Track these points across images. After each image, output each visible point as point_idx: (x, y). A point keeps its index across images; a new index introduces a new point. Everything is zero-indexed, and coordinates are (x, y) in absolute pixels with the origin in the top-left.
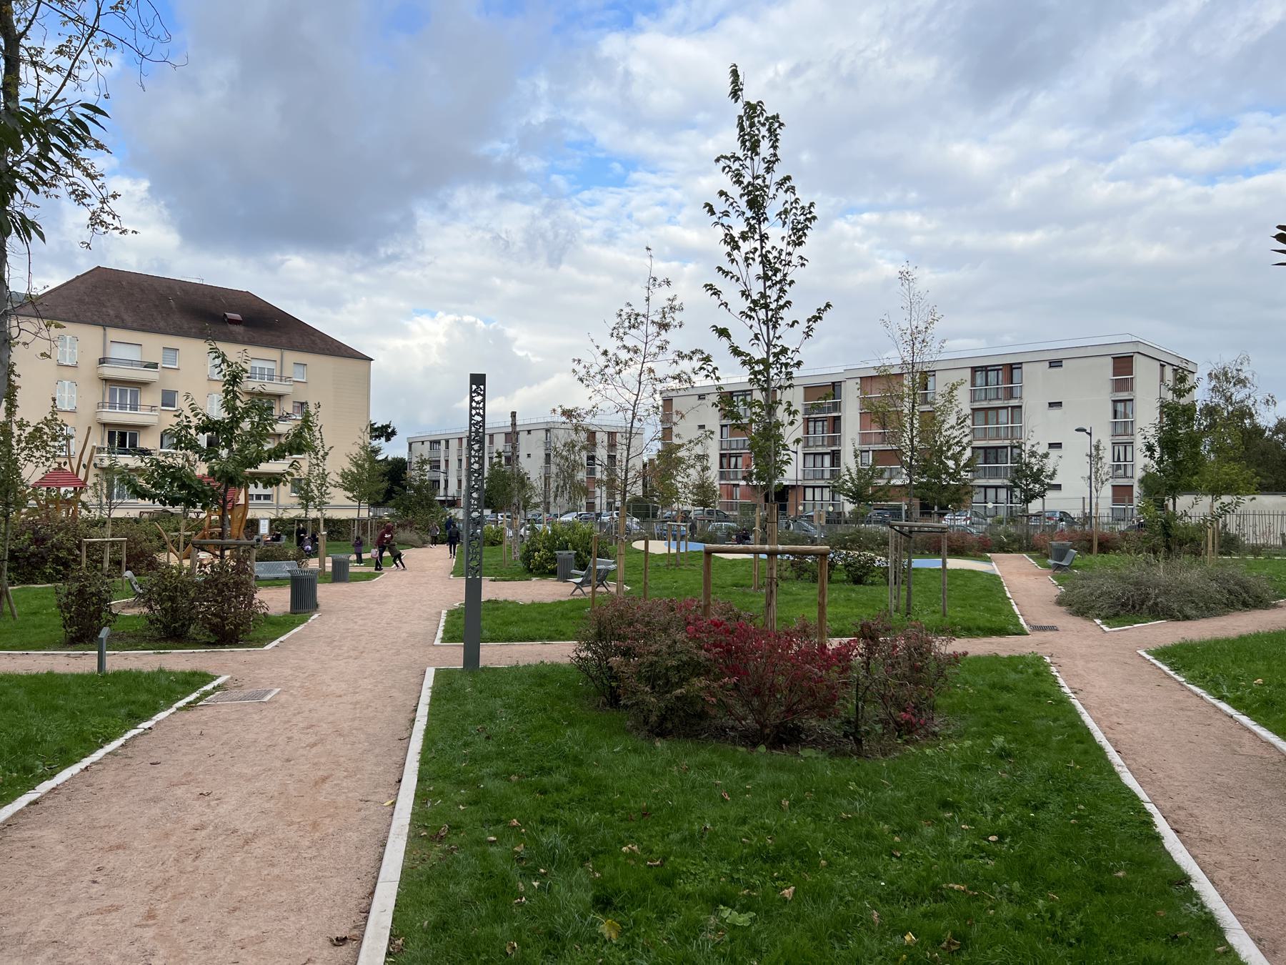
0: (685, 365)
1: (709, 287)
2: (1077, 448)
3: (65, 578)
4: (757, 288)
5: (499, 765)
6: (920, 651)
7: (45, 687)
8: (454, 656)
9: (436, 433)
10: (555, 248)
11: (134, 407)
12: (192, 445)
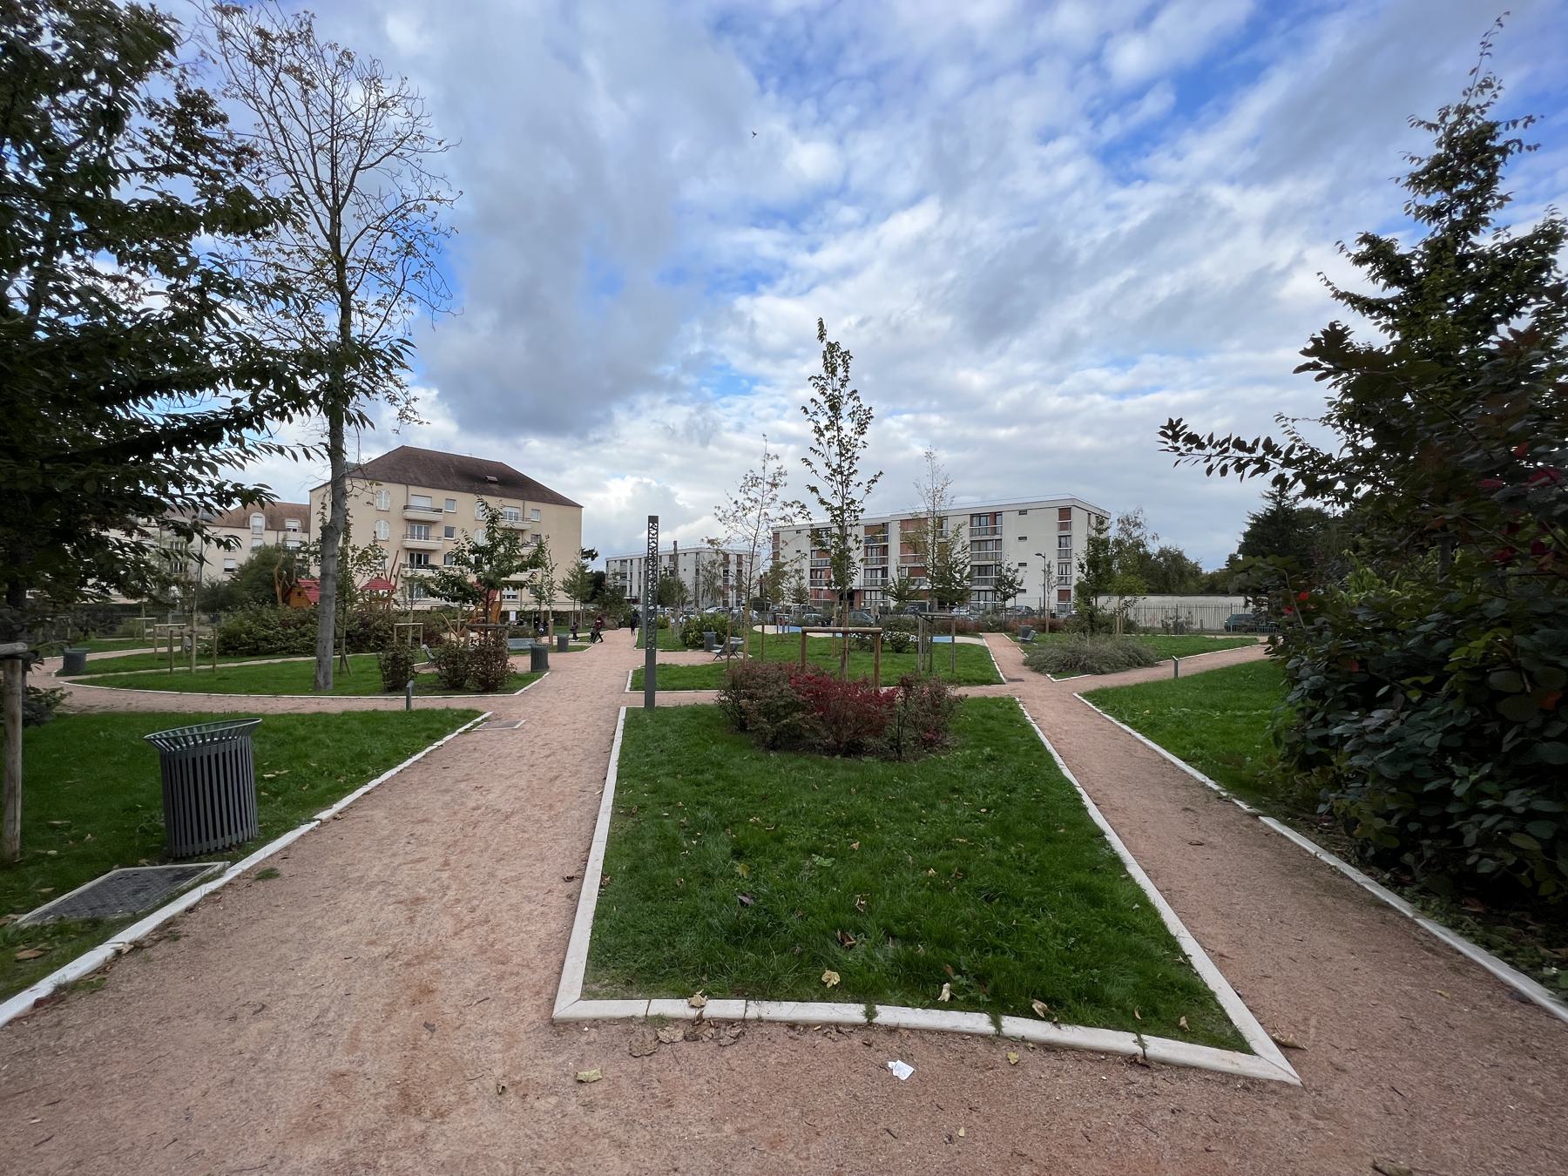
0: (788, 511)
1: (805, 460)
2: (1036, 565)
3: (382, 648)
4: (835, 461)
5: (668, 768)
6: (938, 694)
7: (372, 719)
8: (639, 699)
9: (625, 555)
10: (705, 435)
11: (427, 538)
12: (466, 562)
